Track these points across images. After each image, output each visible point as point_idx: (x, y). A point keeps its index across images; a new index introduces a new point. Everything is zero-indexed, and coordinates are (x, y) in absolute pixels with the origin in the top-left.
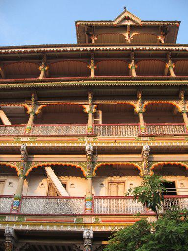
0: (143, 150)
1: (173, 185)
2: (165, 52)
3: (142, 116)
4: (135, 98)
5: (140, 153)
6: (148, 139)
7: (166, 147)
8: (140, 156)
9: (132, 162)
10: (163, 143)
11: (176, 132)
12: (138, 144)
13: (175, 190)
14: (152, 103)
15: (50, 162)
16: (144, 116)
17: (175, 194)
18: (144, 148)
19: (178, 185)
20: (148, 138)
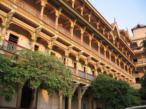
0: (11, 12)
1: (17, 38)
2: (92, 10)
3: (43, 9)
4: (58, 9)
5: (7, 13)
6: (43, 23)
7: (27, 20)
8: (6, 14)
9: (30, 30)
10: (32, 19)
11: (49, 24)
12: (9, 7)
13: (17, 41)
14: (62, 15)
15: (57, 45)
16: (44, 9)
17: (16, 43)
18: (12, 11)
19: (20, 40)
20: (43, 23)
